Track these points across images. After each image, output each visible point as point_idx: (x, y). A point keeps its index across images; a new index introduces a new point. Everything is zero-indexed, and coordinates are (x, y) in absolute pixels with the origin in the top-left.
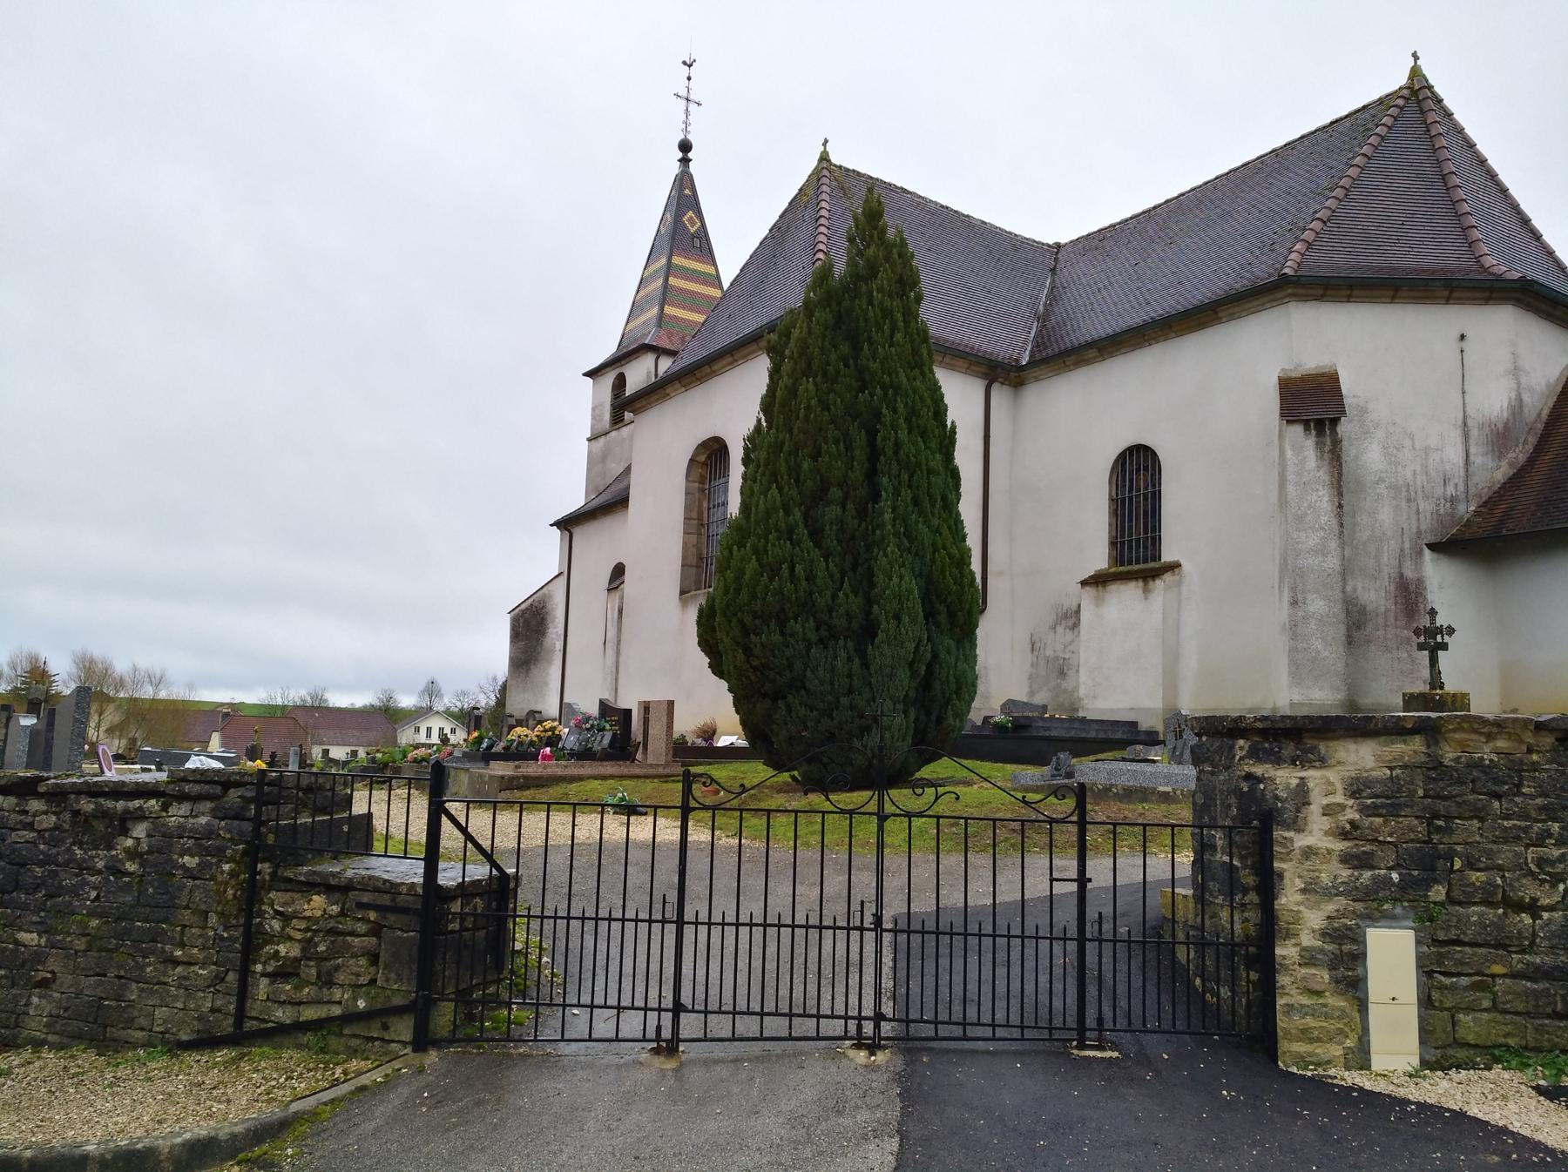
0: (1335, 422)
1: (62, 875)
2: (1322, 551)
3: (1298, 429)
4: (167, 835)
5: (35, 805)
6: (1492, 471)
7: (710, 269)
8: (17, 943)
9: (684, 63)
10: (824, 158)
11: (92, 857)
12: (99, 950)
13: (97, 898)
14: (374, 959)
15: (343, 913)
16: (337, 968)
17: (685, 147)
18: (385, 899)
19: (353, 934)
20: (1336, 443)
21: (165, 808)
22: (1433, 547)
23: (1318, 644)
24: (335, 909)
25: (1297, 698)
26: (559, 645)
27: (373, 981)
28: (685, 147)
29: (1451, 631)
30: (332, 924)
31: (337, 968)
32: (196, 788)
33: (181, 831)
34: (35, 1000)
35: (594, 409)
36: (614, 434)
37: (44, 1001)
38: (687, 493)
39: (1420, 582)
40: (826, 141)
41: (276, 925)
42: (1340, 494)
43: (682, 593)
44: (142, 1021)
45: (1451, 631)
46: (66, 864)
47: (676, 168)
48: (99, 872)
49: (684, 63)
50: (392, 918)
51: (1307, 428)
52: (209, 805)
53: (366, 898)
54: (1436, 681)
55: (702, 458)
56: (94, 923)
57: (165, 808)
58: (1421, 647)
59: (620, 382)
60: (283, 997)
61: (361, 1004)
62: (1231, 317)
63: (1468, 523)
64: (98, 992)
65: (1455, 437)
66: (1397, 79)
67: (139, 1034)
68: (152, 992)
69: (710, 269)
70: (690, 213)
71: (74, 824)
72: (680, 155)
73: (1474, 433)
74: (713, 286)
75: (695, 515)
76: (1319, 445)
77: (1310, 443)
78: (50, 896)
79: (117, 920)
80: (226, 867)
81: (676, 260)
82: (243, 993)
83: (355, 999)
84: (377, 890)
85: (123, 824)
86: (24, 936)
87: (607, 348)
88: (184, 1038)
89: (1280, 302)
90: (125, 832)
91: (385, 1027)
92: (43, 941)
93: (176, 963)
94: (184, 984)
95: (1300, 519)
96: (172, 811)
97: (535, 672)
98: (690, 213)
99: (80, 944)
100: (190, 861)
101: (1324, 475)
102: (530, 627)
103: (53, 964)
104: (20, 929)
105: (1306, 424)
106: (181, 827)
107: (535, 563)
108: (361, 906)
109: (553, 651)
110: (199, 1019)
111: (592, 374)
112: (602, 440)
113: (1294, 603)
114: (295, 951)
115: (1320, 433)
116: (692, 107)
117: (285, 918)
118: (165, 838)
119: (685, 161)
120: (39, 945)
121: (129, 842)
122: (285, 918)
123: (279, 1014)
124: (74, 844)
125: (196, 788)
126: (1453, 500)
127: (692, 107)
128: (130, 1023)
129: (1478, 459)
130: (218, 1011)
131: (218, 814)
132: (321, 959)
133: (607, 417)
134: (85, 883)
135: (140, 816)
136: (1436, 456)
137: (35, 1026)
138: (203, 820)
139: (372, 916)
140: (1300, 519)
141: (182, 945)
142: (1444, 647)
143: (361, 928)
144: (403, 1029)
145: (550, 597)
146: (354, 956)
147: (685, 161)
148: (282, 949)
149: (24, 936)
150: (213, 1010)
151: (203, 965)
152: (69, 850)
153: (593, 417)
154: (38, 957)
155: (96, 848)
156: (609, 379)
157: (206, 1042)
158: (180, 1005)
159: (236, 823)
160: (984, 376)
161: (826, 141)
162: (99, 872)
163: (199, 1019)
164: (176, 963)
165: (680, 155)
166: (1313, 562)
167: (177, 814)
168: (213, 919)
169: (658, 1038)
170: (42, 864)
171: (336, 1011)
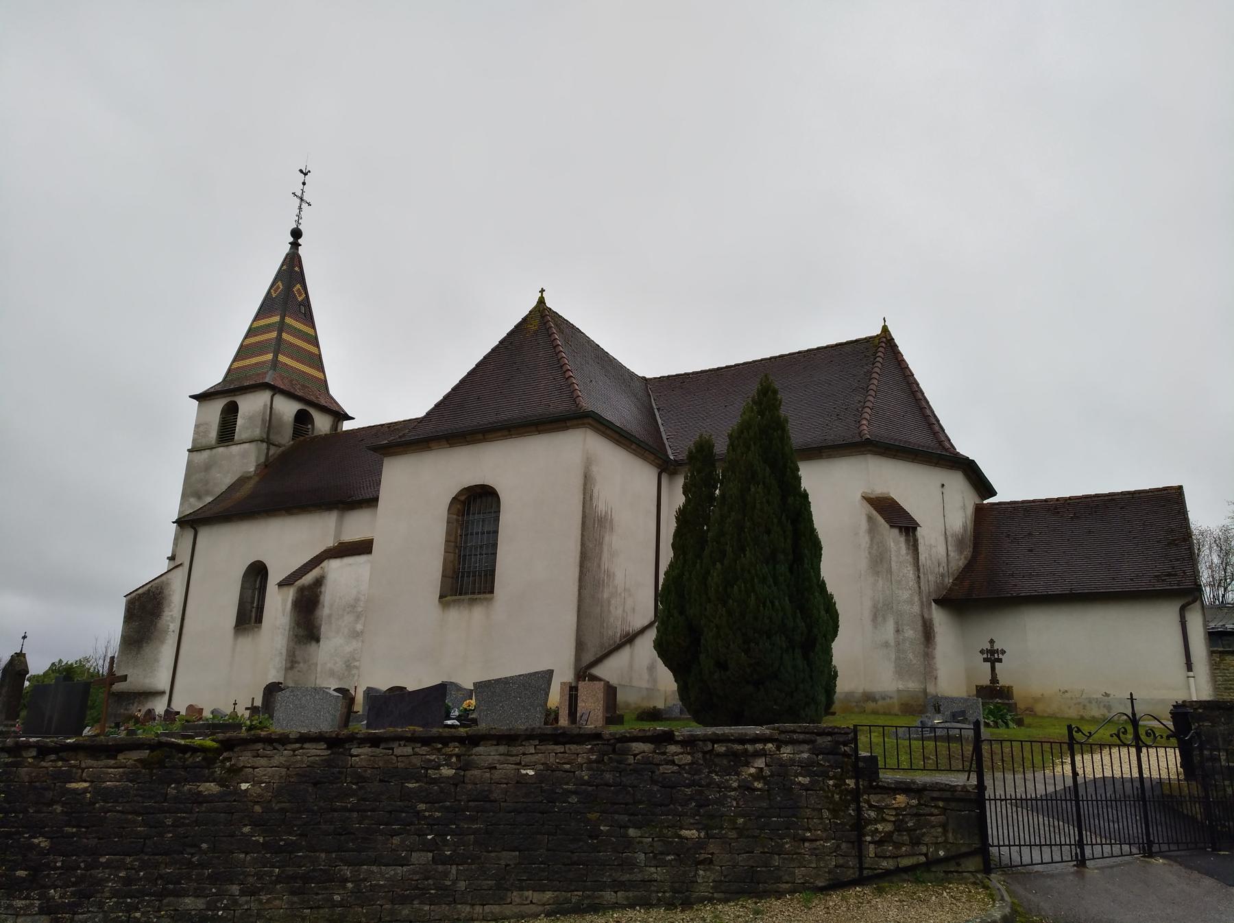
0: (915, 529)
1: (707, 793)
2: (911, 602)
3: (896, 531)
4: (782, 764)
5: (673, 748)
6: (958, 561)
7: (310, 331)
8: (680, 837)
9: (301, 171)
10: (541, 301)
11: (727, 781)
12: (748, 837)
13: (738, 806)
14: (944, 826)
15: (920, 804)
16: (924, 835)
17: (296, 234)
18: (948, 794)
19: (932, 815)
20: (916, 541)
21: (778, 748)
22: (936, 601)
23: (911, 656)
24: (914, 802)
25: (901, 687)
26: (174, 627)
27: (946, 841)
28: (296, 234)
29: (1003, 652)
30: (915, 811)
31: (924, 835)
32: (802, 737)
33: (792, 762)
34: (701, 872)
35: (197, 426)
36: (221, 450)
37: (708, 873)
38: (448, 522)
39: (931, 620)
40: (542, 291)
41: (873, 814)
42: (919, 570)
43: (441, 597)
44: (787, 878)
45: (1003, 652)
46: (708, 785)
47: (287, 248)
48: (735, 789)
49: (301, 171)
50: (953, 805)
51: (901, 531)
52: (806, 747)
53: (935, 794)
54: (994, 679)
55: (463, 498)
56: (741, 821)
57: (778, 748)
58: (985, 660)
59: (231, 412)
60: (888, 854)
61: (941, 853)
62: (829, 457)
63: (951, 589)
64: (751, 863)
65: (942, 539)
66: (876, 331)
67: (787, 886)
68: (793, 860)
69: (310, 331)
70: (298, 286)
71: (704, 759)
72: (291, 239)
73: (950, 539)
74: (309, 342)
75: (453, 539)
76: (907, 541)
77: (902, 539)
78: (700, 806)
79: (760, 817)
80: (831, 782)
81: (288, 320)
82: (860, 857)
83: (937, 851)
84: (941, 790)
85: (743, 759)
86: (685, 833)
87: (214, 376)
88: (821, 884)
89: (862, 453)
90: (747, 764)
91: (958, 864)
92: (702, 835)
93: (805, 840)
94: (813, 852)
95: (899, 582)
96: (782, 750)
97: (147, 650)
98: (298, 286)
99: (733, 835)
100: (805, 780)
101: (910, 558)
102: (145, 610)
103: (712, 848)
104: (681, 828)
105: (900, 528)
106: (791, 759)
107: (149, 556)
108: (933, 799)
109: (166, 632)
110: (829, 872)
111: (201, 398)
112: (206, 454)
113: (898, 631)
114: (889, 827)
115: (907, 534)
116: (304, 206)
117: (879, 809)
118: (782, 769)
119: (295, 245)
120: (699, 837)
121: (752, 770)
122: (879, 809)
123: (885, 864)
124: (710, 772)
125: (802, 737)
126: (942, 575)
127: (304, 206)
128: (779, 880)
129: (952, 554)
130: (841, 866)
131: (816, 751)
132: (909, 830)
133: (213, 434)
134: (726, 797)
135: (757, 754)
136: (934, 550)
137: (703, 889)
138: (805, 755)
139: (941, 804)
140: (899, 582)
141: (809, 830)
142: (1000, 660)
143: (936, 811)
144: (972, 864)
145: (168, 584)
146: (933, 827)
147: (295, 245)
148: (880, 827)
149: (685, 833)
150: (836, 866)
151: (826, 840)
152: (708, 776)
153: (196, 432)
154: (700, 845)
155: (729, 774)
156: (218, 406)
157: (837, 885)
158: (814, 865)
159: (831, 757)
160: (658, 466)
161: (542, 291)
162: (735, 789)
163: (829, 872)
164: (805, 840)
165: (291, 239)
166: (906, 607)
167: (786, 752)
168: (826, 814)
169: (1077, 859)
170: (688, 786)
171: (923, 859)
